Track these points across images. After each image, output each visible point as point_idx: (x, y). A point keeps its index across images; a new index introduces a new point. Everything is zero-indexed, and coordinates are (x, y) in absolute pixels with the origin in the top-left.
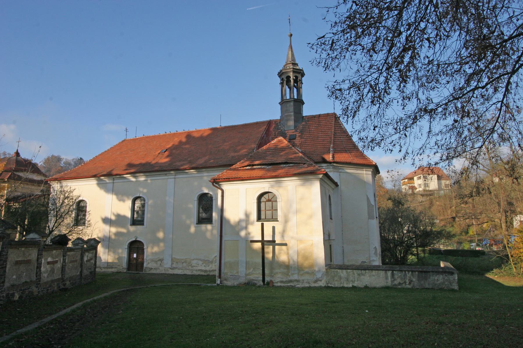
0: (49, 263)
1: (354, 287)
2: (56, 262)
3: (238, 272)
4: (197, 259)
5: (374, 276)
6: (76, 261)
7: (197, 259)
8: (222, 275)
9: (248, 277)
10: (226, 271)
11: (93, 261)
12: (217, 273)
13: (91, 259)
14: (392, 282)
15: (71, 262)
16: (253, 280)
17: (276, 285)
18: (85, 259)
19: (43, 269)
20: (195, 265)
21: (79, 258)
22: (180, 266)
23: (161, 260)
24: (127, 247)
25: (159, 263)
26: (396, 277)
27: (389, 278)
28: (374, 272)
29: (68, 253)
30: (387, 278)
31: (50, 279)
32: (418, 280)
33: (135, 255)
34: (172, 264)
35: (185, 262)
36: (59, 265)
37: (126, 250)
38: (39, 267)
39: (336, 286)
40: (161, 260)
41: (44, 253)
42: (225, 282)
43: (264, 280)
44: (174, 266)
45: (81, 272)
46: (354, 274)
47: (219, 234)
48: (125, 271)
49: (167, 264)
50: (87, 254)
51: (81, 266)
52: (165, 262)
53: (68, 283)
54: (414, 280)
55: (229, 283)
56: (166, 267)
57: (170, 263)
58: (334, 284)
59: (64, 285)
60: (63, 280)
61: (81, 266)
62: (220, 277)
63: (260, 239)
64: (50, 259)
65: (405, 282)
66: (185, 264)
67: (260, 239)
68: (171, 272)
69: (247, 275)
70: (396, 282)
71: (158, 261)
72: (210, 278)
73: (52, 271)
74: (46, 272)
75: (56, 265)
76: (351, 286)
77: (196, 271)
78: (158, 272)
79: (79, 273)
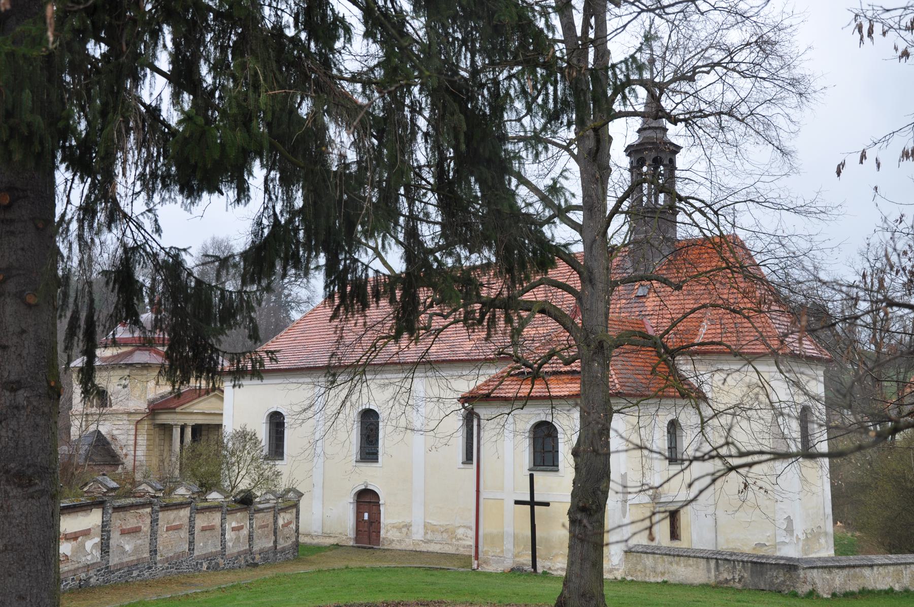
0: (233, 529)
1: (665, 582)
2: (241, 528)
3: (502, 551)
4: (464, 527)
5: (690, 566)
6: (267, 526)
7: (464, 527)
8: (481, 555)
9: (518, 559)
10: (485, 549)
11: (293, 526)
12: (473, 554)
13: (290, 523)
14: (716, 577)
15: (261, 527)
16: (523, 564)
17: (555, 573)
18: (281, 522)
19: (227, 537)
20: (461, 536)
21: (271, 520)
22: (439, 537)
23: (408, 526)
24: (352, 501)
25: (404, 530)
26: (722, 569)
27: (713, 571)
28: (691, 561)
29: (256, 515)
30: (709, 571)
31: (236, 550)
32: (752, 576)
33: (366, 516)
34: (426, 533)
35: (446, 531)
36: (245, 532)
37: (352, 506)
38: (223, 535)
39: (640, 579)
40: (408, 526)
41: (228, 517)
42: (484, 566)
43: (534, 565)
44: (429, 537)
45: (275, 542)
46: (664, 561)
47: (475, 489)
48: (351, 543)
49: (418, 534)
50: (282, 514)
51: (275, 533)
52: (414, 529)
53: (257, 557)
54: (746, 575)
55: (490, 569)
56: (417, 538)
57: (422, 531)
58: (637, 576)
59: (253, 559)
60: (250, 551)
61: (275, 533)
62: (477, 558)
63: (528, 499)
64: (234, 524)
65: (734, 579)
66: (445, 535)
67: (528, 499)
68: (424, 548)
69: (515, 556)
70: (721, 578)
71: (403, 526)
72: (465, 561)
73: (238, 538)
74: (231, 540)
75: (241, 531)
76: (660, 580)
77: (464, 547)
78: (403, 546)
79: (271, 544)
